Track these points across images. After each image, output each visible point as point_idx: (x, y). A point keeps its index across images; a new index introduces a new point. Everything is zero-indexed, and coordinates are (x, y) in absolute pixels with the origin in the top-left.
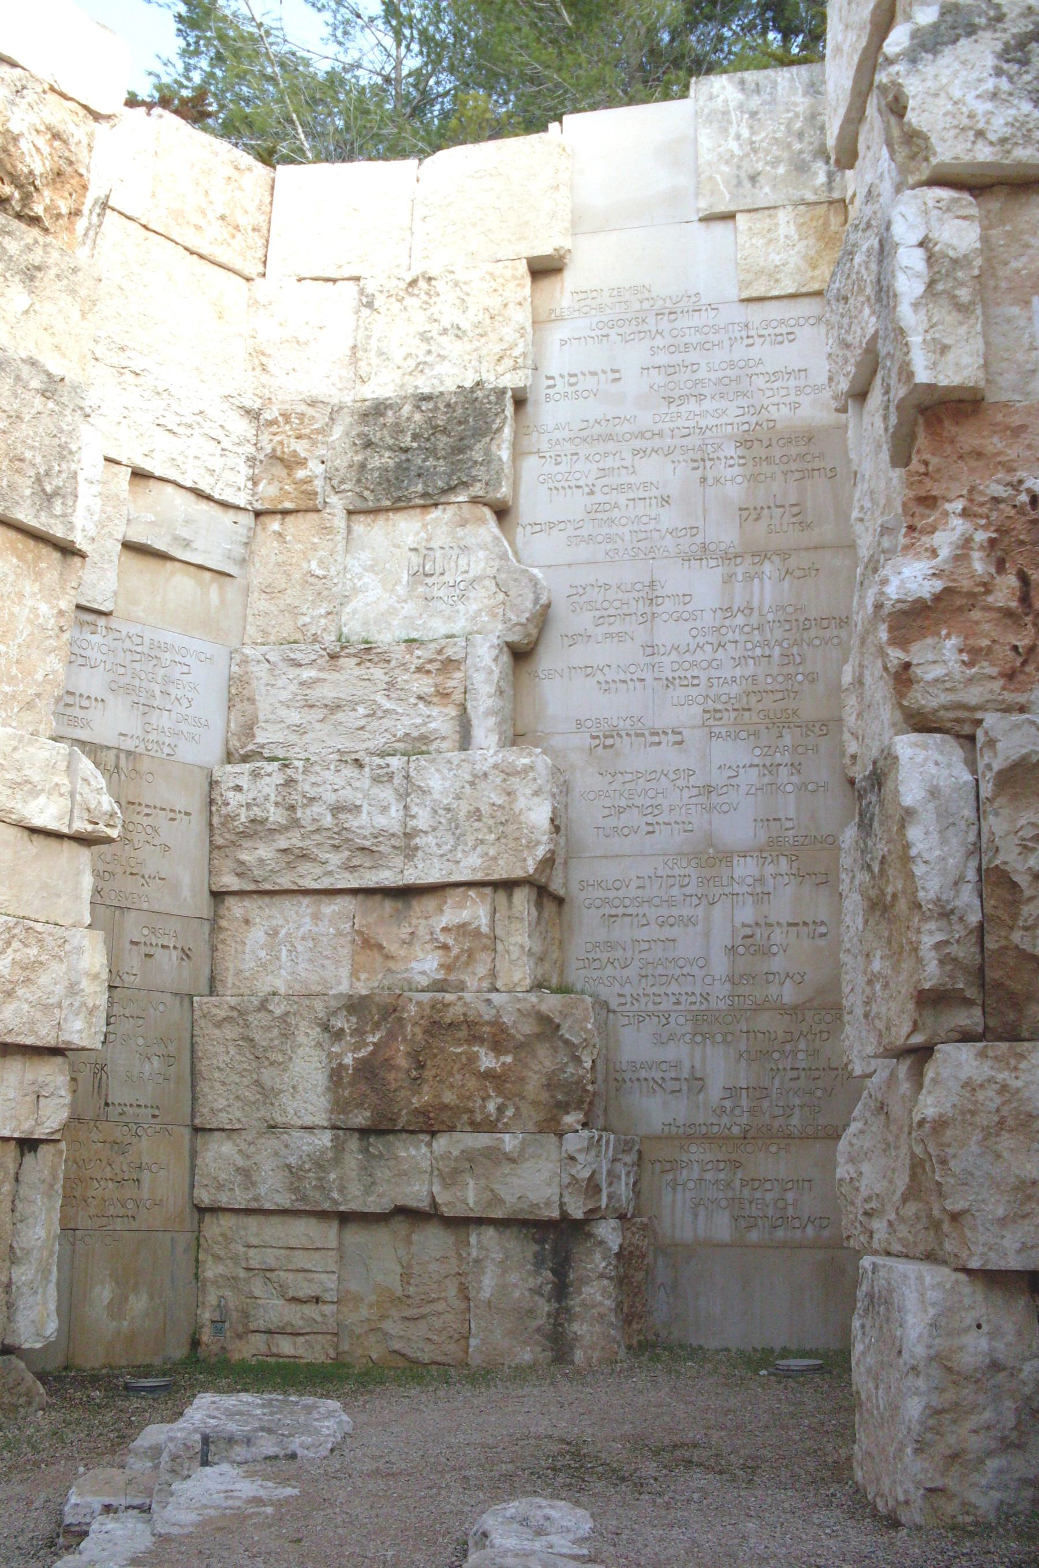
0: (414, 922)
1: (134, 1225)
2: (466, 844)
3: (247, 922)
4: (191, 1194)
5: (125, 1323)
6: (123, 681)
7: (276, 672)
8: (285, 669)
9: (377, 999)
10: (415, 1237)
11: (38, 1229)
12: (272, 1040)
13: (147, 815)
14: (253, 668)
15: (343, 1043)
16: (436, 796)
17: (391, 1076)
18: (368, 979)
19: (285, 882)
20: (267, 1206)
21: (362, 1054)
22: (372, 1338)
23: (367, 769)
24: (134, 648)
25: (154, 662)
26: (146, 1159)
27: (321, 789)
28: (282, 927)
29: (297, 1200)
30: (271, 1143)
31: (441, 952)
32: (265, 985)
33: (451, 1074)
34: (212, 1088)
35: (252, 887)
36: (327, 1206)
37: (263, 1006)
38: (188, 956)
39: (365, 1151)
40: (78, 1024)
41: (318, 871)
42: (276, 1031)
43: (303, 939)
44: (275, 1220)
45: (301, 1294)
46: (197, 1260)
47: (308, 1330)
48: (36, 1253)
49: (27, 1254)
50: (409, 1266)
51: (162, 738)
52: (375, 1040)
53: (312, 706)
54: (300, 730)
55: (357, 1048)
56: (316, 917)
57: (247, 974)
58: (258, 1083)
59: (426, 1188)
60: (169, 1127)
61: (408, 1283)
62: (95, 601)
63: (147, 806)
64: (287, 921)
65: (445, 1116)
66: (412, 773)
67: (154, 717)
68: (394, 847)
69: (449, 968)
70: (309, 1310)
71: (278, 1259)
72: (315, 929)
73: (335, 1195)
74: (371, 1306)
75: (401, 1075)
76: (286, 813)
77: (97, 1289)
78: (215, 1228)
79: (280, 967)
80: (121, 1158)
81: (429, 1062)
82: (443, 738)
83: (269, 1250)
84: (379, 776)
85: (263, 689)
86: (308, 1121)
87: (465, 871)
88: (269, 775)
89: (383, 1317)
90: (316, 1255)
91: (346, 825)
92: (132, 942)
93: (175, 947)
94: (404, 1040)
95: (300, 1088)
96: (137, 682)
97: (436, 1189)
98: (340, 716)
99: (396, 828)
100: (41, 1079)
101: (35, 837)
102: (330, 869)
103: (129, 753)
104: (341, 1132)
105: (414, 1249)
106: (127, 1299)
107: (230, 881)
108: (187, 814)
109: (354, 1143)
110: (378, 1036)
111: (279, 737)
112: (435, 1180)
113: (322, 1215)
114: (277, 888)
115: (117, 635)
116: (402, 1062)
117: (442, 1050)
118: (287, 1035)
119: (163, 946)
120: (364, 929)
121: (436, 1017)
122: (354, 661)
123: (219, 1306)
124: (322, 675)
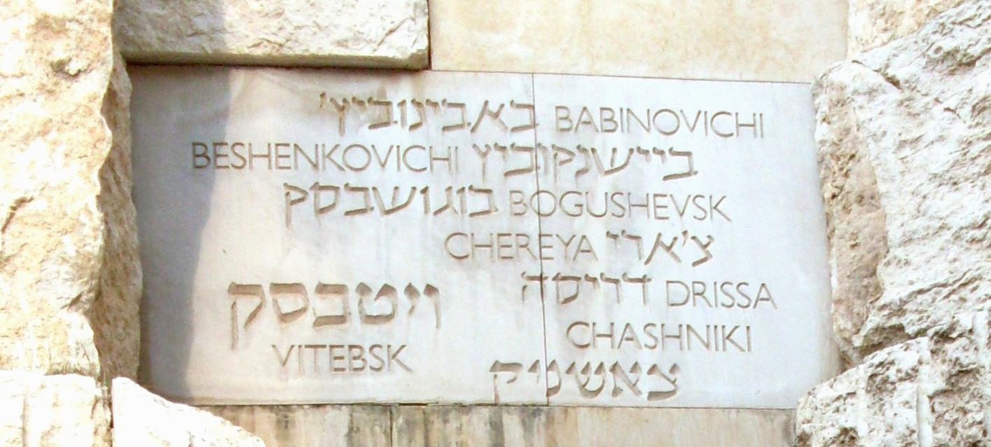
6: (485, 229)
7: (918, 105)
8: (936, 90)
14: (862, 113)
24: (506, 141)
51: (626, 356)
62: (358, 38)
85: (891, 159)
88: (911, 376)
96: (530, 225)
103: (530, 411)
115: (454, 116)
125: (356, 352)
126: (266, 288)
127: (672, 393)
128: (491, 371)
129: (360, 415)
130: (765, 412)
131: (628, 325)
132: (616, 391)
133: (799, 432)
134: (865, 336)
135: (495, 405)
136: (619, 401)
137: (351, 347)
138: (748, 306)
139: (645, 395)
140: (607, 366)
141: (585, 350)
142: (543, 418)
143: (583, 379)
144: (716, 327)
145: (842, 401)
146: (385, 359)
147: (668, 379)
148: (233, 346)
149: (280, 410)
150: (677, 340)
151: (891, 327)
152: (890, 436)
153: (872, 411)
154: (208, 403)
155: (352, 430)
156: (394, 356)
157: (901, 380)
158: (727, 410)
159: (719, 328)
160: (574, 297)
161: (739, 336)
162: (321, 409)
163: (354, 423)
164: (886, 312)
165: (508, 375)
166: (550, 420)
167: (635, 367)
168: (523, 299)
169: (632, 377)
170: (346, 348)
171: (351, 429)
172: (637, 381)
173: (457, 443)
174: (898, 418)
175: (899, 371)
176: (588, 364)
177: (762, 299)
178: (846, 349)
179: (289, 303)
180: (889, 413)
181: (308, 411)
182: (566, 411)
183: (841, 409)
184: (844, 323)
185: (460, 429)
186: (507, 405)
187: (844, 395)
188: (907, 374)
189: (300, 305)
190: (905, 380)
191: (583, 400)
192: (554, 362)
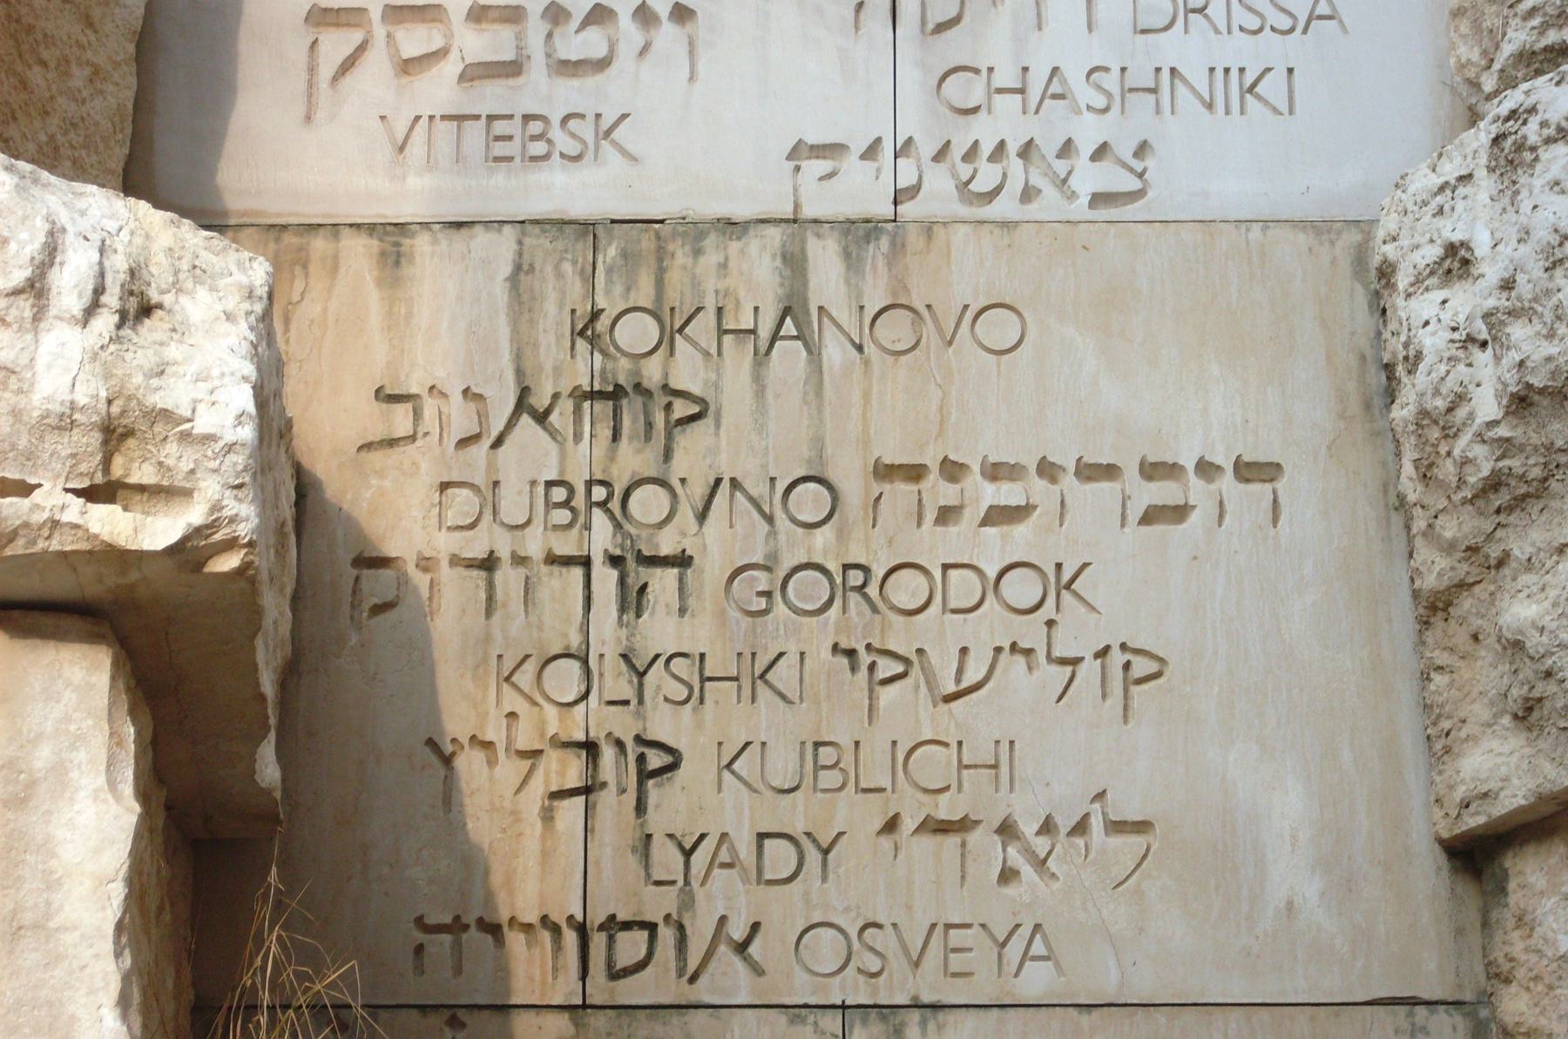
13: (999, 515)
51: (1048, 130)
63: (995, 472)
103: (859, 233)
108: (1247, 471)
125: (535, 127)
126: (376, 14)
127: (1139, 194)
128: (789, 158)
129: (538, 242)
130: (1320, 228)
131: (1055, 70)
132: (1028, 194)
133: (1376, 261)
134: (1502, 70)
135: (795, 221)
136: (1033, 210)
137: (527, 118)
138: (1292, 30)
139: (1084, 200)
140: (1013, 147)
141: (970, 117)
142: (884, 243)
143: (965, 171)
144: (1227, 70)
145: (1448, 192)
146: (589, 138)
147: (1131, 170)
148: (308, 118)
149: (386, 233)
150: (1151, 98)
151: (1545, 49)
152: (1524, 249)
153: (1498, 206)
154: (253, 221)
155: (520, 270)
156: (608, 133)
157: (1548, 141)
158: (1243, 226)
159: (1234, 73)
160: (956, 20)
161: (1273, 87)
162: (464, 231)
163: (526, 256)
164: (1536, 22)
165: (822, 166)
166: (898, 247)
167: (1067, 149)
168: (857, 28)
169: (1061, 167)
170: (518, 120)
171: (518, 268)
172: (1070, 173)
173: (717, 292)
174: (1540, 213)
175: (1544, 124)
176: (976, 142)
177: (1320, 17)
178: (1473, 101)
179: (415, 40)
180: (1526, 207)
181: (440, 235)
182: (930, 229)
183: (1446, 208)
184: (1470, 52)
185: (724, 266)
186: (816, 221)
187: (1453, 182)
188: (1560, 129)
189: (438, 43)
190: (1556, 141)
191: (964, 211)
192: (910, 141)
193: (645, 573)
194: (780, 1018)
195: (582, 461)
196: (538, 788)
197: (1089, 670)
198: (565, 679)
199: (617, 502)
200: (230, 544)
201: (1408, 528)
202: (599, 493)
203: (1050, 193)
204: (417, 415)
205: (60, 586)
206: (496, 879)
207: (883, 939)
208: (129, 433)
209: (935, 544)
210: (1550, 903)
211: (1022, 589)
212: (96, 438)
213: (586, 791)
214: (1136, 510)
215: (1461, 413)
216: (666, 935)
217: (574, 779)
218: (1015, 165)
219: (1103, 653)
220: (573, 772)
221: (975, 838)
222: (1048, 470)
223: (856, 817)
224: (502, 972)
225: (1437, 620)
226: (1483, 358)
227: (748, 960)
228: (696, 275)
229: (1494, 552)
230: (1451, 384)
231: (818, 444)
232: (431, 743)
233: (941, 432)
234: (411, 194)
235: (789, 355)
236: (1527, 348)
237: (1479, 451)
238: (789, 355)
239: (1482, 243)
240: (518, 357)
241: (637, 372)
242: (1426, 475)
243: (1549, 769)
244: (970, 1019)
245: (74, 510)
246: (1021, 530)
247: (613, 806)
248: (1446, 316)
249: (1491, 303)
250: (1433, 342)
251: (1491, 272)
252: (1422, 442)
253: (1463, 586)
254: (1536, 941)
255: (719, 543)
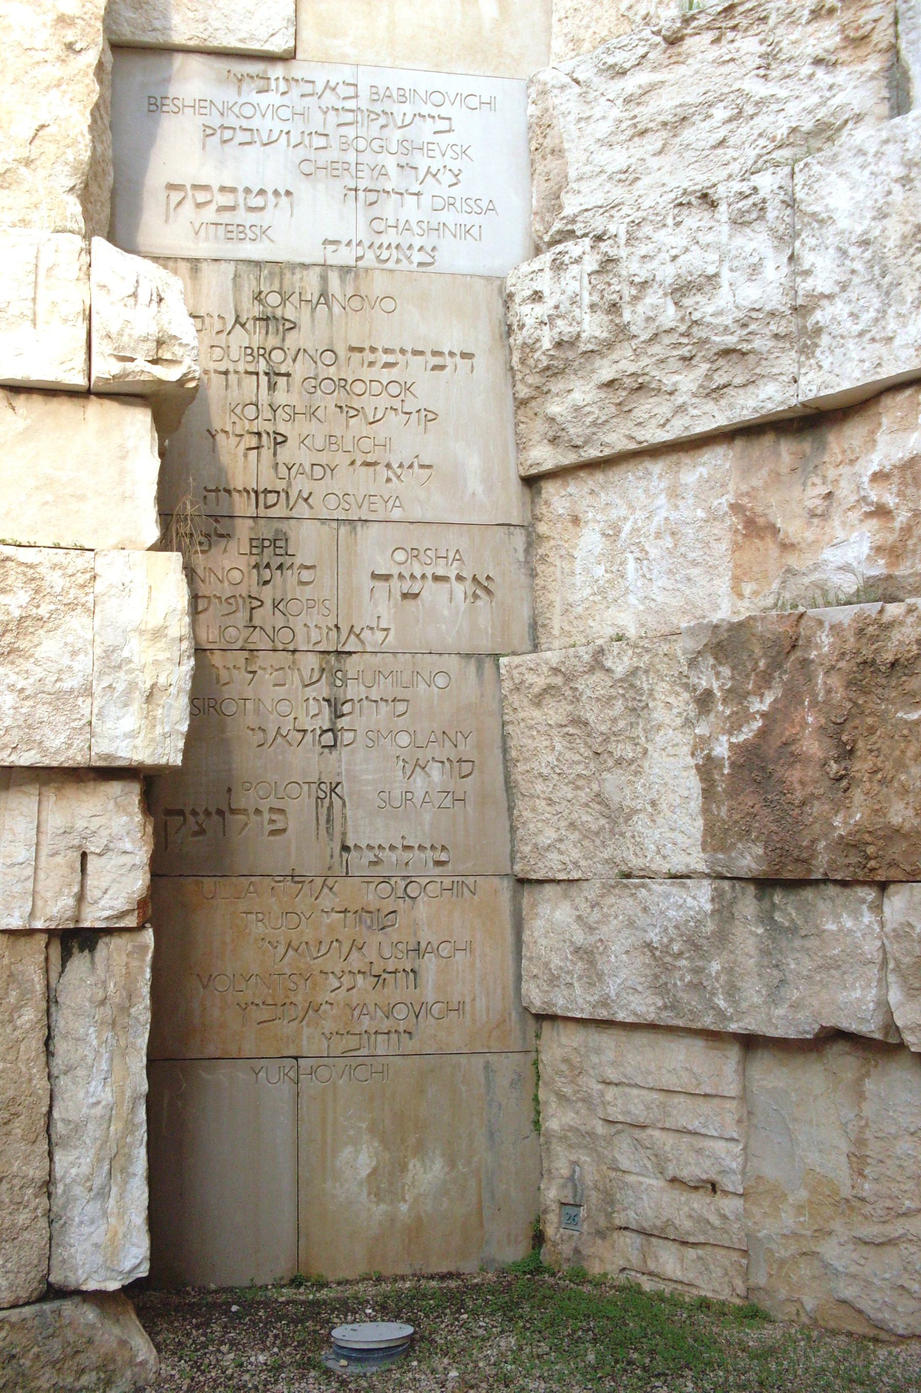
0: (831, 473)
1: (410, 1046)
2: (903, 301)
3: (576, 520)
4: (518, 988)
5: (404, 1207)
6: (324, 158)
8: (602, 88)
9: (760, 628)
10: (869, 1085)
11: (95, 1085)
12: (614, 720)
13: (387, 365)
15: (712, 717)
16: (843, 223)
17: (794, 775)
18: (755, 593)
19: (617, 440)
20: (621, 1016)
21: (746, 734)
22: (805, 1270)
23: (723, 208)
25: (382, 121)
26: (426, 936)
27: (655, 263)
28: (626, 519)
29: (665, 1007)
30: (623, 904)
31: (874, 523)
32: (602, 628)
33: (900, 765)
34: (534, 810)
35: (570, 458)
36: (708, 1021)
37: (597, 663)
38: (488, 591)
39: (766, 918)
40: (130, 720)
41: (664, 409)
42: (619, 704)
43: (658, 535)
44: (641, 1039)
45: (684, 1174)
46: (536, 1100)
47: (702, 1239)
48: (93, 1131)
49: (76, 1130)
50: (860, 1142)
51: (405, 240)
52: (765, 708)
53: (643, 133)
54: (628, 177)
55: (734, 726)
56: (674, 493)
57: (580, 610)
58: (598, 797)
59: (873, 993)
60: (470, 881)
61: (861, 1174)
63: (386, 351)
64: (632, 507)
65: (897, 850)
66: (800, 195)
67: (388, 208)
68: (776, 336)
69: (892, 552)
70: (699, 1203)
71: (648, 1108)
72: (674, 515)
73: (721, 1002)
74: (800, 1209)
75: (812, 772)
76: (606, 318)
77: (346, 1153)
78: (558, 1046)
79: (627, 591)
80: (380, 937)
81: (860, 744)
82: (858, 118)
83: (635, 1091)
84: (742, 213)
85: (573, 128)
86: (678, 863)
87: (904, 354)
88: (578, 261)
89: (824, 1233)
90: (706, 1107)
91: (696, 316)
92: (374, 576)
93: (459, 578)
94: (814, 703)
95: (664, 806)
96: (351, 157)
97: (895, 996)
98: (688, 134)
99: (775, 299)
100: (80, 824)
101: (21, 401)
102: (680, 401)
103: (345, 270)
104: (726, 885)
105: (868, 1109)
106: (404, 1168)
107: (544, 457)
108: (465, 355)
109: (748, 905)
110: (769, 698)
111: (598, 198)
112: (892, 978)
113: (713, 1036)
114: (607, 452)
116: (812, 746)
117: (883, 717)
118: (637, 710)
119: (436, 578)
120: (745, 501)
121: (867, 653)
122: (710, 36)
123: (571, 1178)
124: (657, 77)
125: (241, 229)
126: (188, 187)
127: (432, 263)
129: (241, 267)
130: (488, 279)
132: (398, 261)
136: (400, 266)
140: (393, 245)
142: (353, 274)
143: (378, 252)
148: (166, 221)
160: (375, 202)
165: (333, 247)
166: (357, 276)
167: (410, 247)
169: (408, 253)
171: (235, 276)
179: (201, 197)
180: (563, 283)
185: (302, 279)
189: (209, 198)
191: (377, 265)
193: (275, 379)
194: (318, 523)
195: (256, 340)
196: (242, 447)
197: (414, 416)
198: (251, 411)
199: (267, 354)
200: (193, 379)
201: (513, 377)
202: (262, 351)
203: (405, 261)
204: (203, 323)
205: (137, 389)
206: (230, 475)
207: (350, 499)
208: (164, 343)
209: (367, 374)
210: (556, 498)
211: (394, 389)
212: (155, 344)
213: (257, 448)
214: (430, 366)
215: (538, 345)
216: (283, 495)
217: (254, 445)
218: (394, 251)
219: (418, 411)
220: (254, 442)
221: (378, 468)
222: (403, 351)
223: (342, 460)
224: (232, 505)
225: (522, 407)
226: (546, 328)
227: (308, 504)
228: (293, 281)
229: (545, 389)
230: (535, 335)
231: (331, 338)
232: (208, 431)
233: (370, 338)
234: (202, 249)
235: (322, 309)
236: (562, 328)
237: (543, 358)
238: (322, 309)
239: (546, 293)
240: (236, 305)
241: (273, 313)
242: (523, 361)
243: (561, 458)
244: (376, 525)
245: (149, 367)
246: (394, 370)
247: (266, 453)
248: (534, 314)
249: (551, 312)
250: (529, 321)
251: (550, 302)
252: (523, 352)
253: (533, 398)
254: (551, 509)
255: (300, 370)
